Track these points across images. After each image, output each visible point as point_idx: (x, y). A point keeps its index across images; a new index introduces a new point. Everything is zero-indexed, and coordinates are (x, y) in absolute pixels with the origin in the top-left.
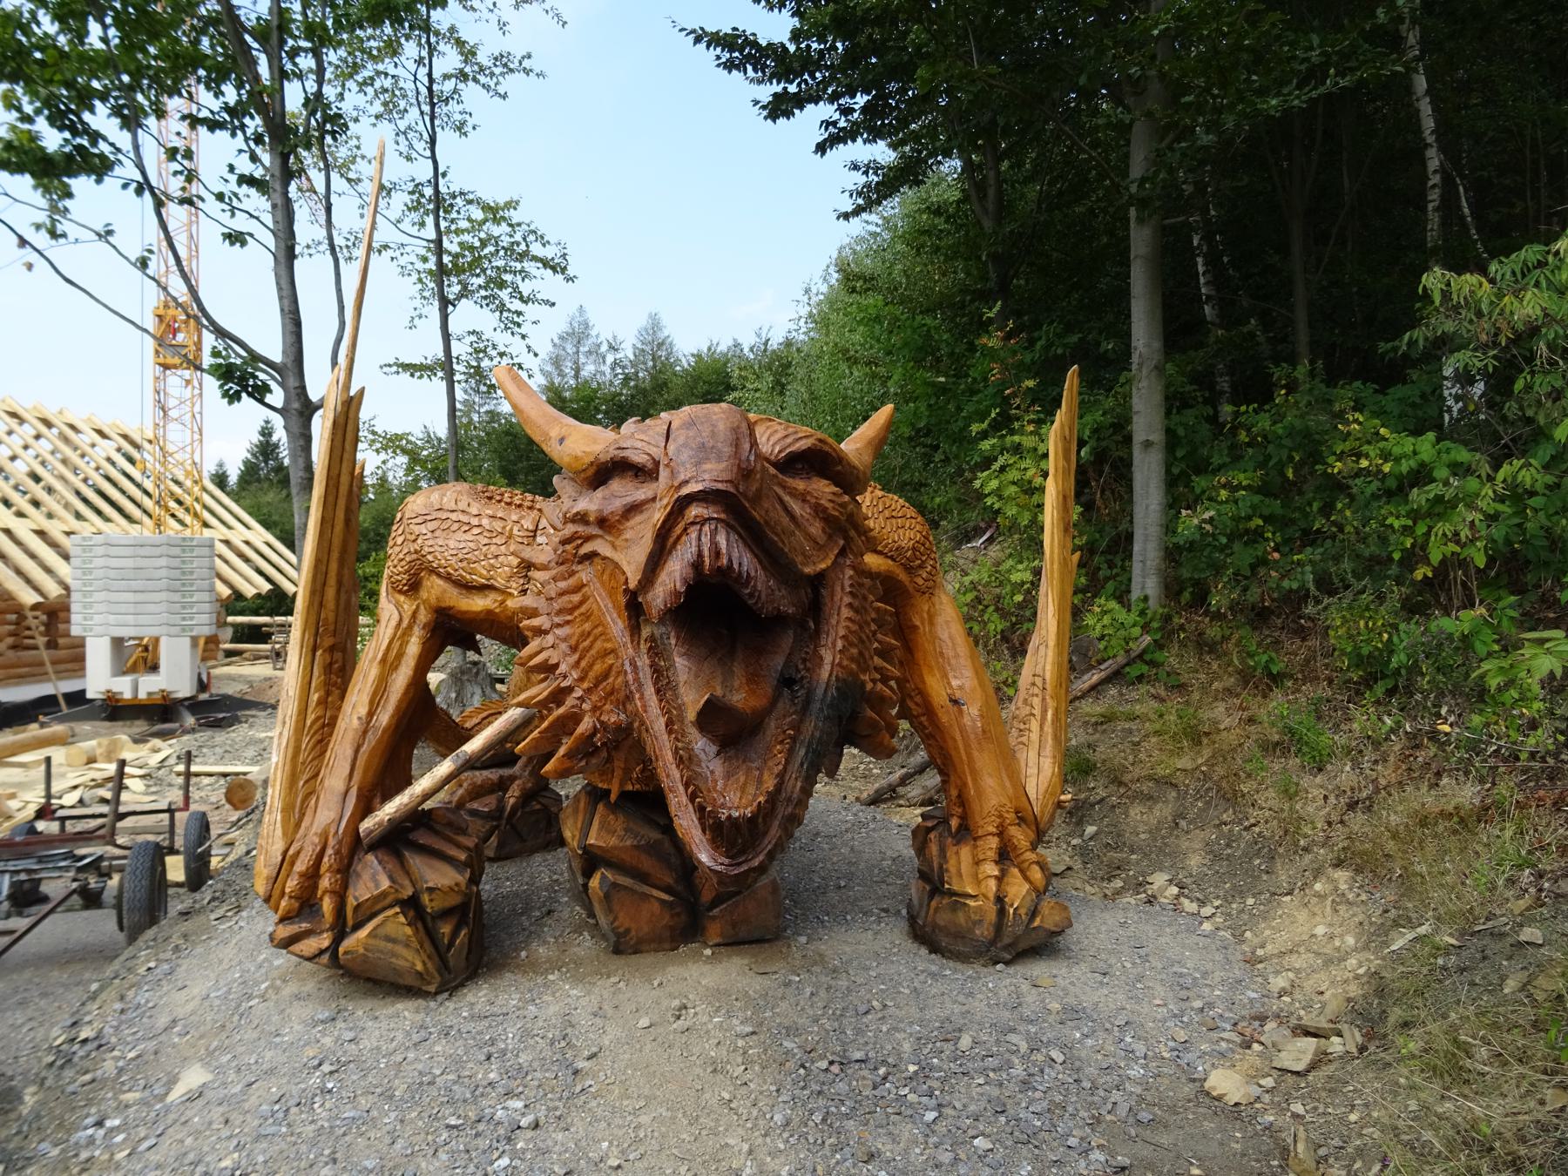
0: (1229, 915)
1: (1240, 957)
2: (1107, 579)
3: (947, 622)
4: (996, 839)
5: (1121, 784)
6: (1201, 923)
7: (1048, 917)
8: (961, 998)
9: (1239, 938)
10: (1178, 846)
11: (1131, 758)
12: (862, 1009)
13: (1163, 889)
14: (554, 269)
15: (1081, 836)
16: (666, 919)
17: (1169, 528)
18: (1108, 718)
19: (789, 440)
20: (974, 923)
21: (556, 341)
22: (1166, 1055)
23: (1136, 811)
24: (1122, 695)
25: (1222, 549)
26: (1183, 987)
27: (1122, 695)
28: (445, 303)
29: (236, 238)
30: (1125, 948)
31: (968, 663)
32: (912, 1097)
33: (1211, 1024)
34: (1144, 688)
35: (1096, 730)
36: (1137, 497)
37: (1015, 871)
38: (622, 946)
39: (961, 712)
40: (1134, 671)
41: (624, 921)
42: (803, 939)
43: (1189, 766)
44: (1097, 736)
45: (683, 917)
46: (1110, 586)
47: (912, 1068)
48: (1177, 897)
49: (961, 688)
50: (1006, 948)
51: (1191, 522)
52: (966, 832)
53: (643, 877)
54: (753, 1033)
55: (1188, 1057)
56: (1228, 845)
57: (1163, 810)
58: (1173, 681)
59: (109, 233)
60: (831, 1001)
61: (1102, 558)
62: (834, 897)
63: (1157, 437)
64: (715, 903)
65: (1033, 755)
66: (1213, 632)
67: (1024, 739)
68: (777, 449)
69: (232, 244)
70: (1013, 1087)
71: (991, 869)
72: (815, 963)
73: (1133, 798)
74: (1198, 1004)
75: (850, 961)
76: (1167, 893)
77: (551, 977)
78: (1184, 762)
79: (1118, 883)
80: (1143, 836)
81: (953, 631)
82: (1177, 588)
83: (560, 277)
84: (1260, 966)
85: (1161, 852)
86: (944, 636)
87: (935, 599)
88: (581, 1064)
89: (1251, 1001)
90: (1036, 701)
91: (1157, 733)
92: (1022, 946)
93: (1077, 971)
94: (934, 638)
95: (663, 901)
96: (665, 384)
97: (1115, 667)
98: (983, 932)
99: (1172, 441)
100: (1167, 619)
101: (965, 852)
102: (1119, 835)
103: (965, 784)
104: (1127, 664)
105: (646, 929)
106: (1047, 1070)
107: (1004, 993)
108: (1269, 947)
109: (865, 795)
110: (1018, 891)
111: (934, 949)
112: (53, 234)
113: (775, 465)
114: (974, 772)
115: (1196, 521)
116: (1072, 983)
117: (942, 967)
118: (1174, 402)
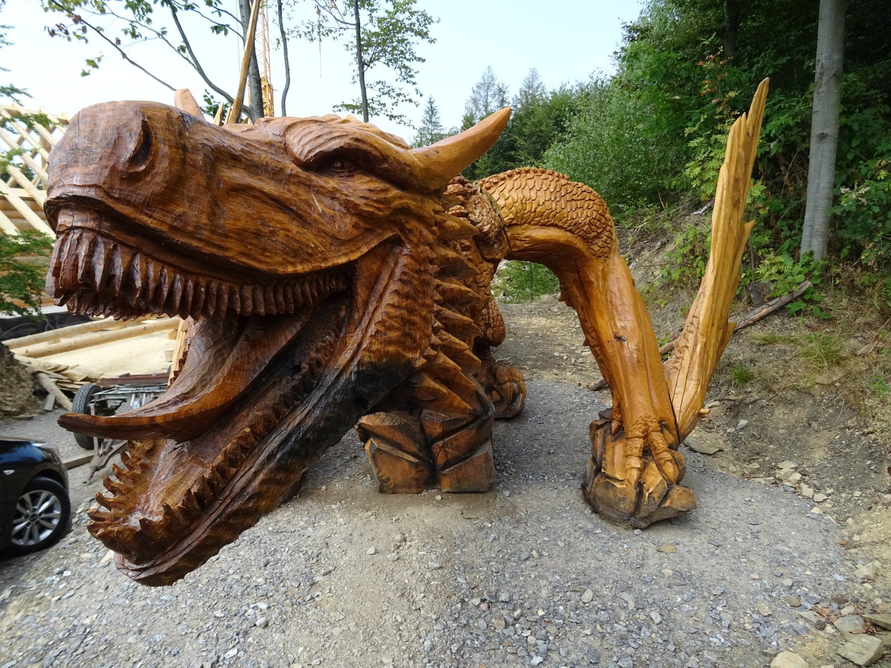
0: (838, 502)
1: (838, 540)
2: (786, 238)
3: (617, 278)
4: (642, 440)
5: (771, 391)
6: (812, 507)
7: (678, 500)
8: (600, 555)
9: (842, 522)
10: (808, 441)
11: (781, 372)
12: (524, 557)
13: (787, 475)
14: (420, 35)
15: (735, 426)
16: (413, 474)
17: (836, 200)
18: (770, 342)
19: (321, 141)
20: (620, 499)
21: (475, 89)
22: (748, 626)
23: (780, 412)
24: (783, 324)
25: (875, 216)
26: (779, 563)
27: (783, 324)
28: (362, 64)
29: (217, 28)
30: (743, 525)
31: (631, 310)
32: (532, 640)
33: (795, 601)
34: (800, 320)
35: (759, 350)
36: (810, 178)
37: (654, 465)
38: (385, 488)
39: (622, 346)
40: (794, 307)
41: (385, 473)
42: (507, 493)
43: (826, 382)
44: (759, 353)
45: (426, 473)
46: (787, 243)
47: (541, 613)
48: (799, 482)
49: (624, 328)
50: (643, 519)
51: (850, 197)
52: (620, 433)
53: (399, 447)
54: (441, 568)
55: (767, 631)
56: (848, 446)
57: (800, 413)
58: (824, 315)
59: (164, 33)
60: (505, 546)
61: (777, 222)
62: (542, 460)
63: (831, 130)
64: (447, 464)
65: (682, 376)
66: (861, 279)
67: (677, 365)
68: (307, 148)
69: (218, 33)
70: (611, 640)
71: (636, 463)
72: (507, 514)
73: (779, 402)
74: (788, 582)
75: (532, 514)
76: (791, 478)
77: (333, 507)
78: (822, 379)
79: (756, 465)
80: (781, 431)
81: (622, 285)
82: (838, 245)
83: (426, 40)
84: (853, 551)
85: (794, 446)
86: (615, 289)
87: (610, 261)
88: (318, 578)
89: (837, 583)
90: (691, 337)
91: (807, 354)
92: (656, 518)
93: (697, 541)
94: (606, 291)
95: (411, 463)
96: (533, 112)
97: (780, 304)
98: (626, 506)
99: (845, 134)
100: (827, 268)
101: (619, 448)
102: (762, 429)
103: (622, 399)
104: (791, 302)
105: (400, 479)
106: (643, 629)
107: (633, 554)
108: (865, 535)
109: (592, 384)
110: (654, 481)
111: (595, 511)
112: (134, 35)
113: (297, 162)
114: (629, 391)
115: (854, 196)
116: (689, 551)
117: (596, 526)
118: (849, 103)
